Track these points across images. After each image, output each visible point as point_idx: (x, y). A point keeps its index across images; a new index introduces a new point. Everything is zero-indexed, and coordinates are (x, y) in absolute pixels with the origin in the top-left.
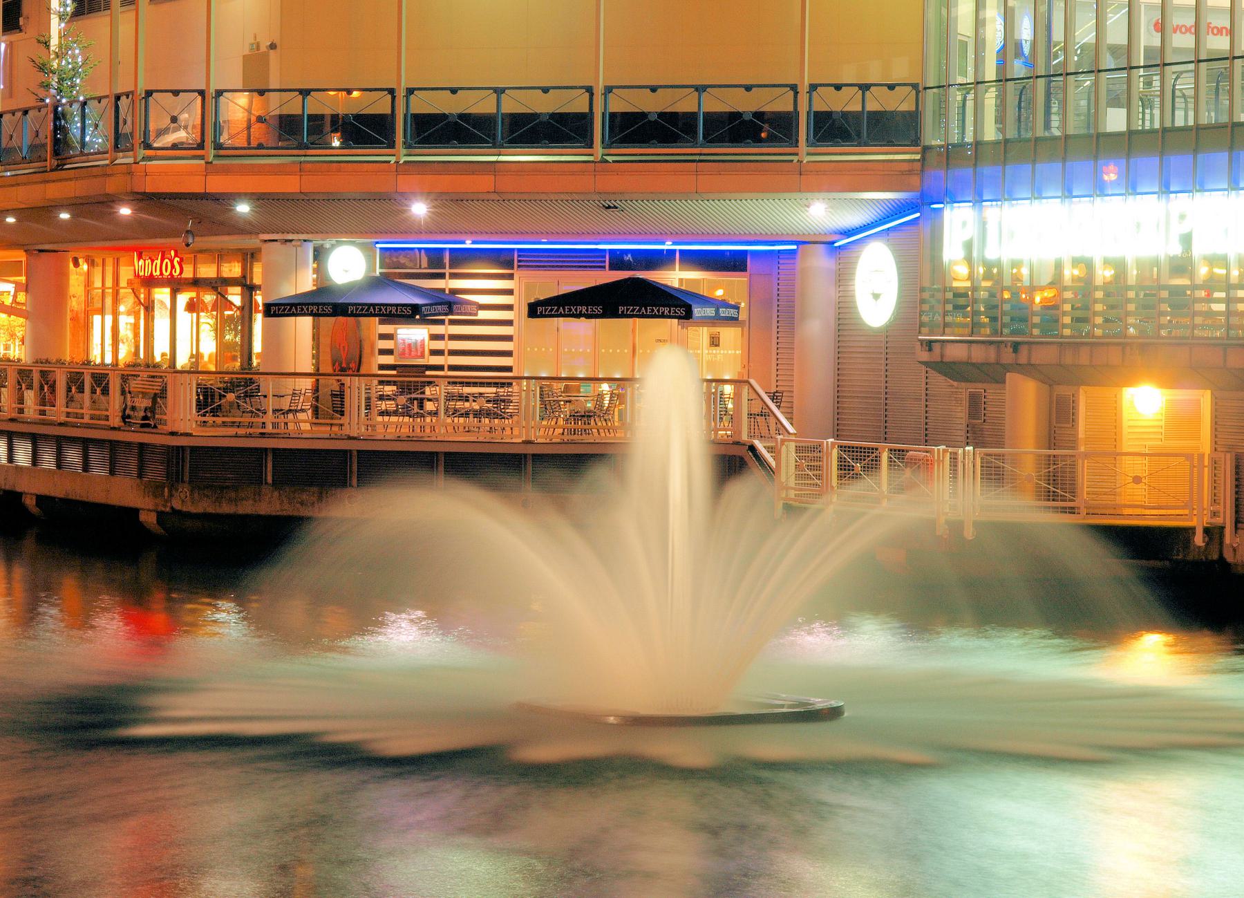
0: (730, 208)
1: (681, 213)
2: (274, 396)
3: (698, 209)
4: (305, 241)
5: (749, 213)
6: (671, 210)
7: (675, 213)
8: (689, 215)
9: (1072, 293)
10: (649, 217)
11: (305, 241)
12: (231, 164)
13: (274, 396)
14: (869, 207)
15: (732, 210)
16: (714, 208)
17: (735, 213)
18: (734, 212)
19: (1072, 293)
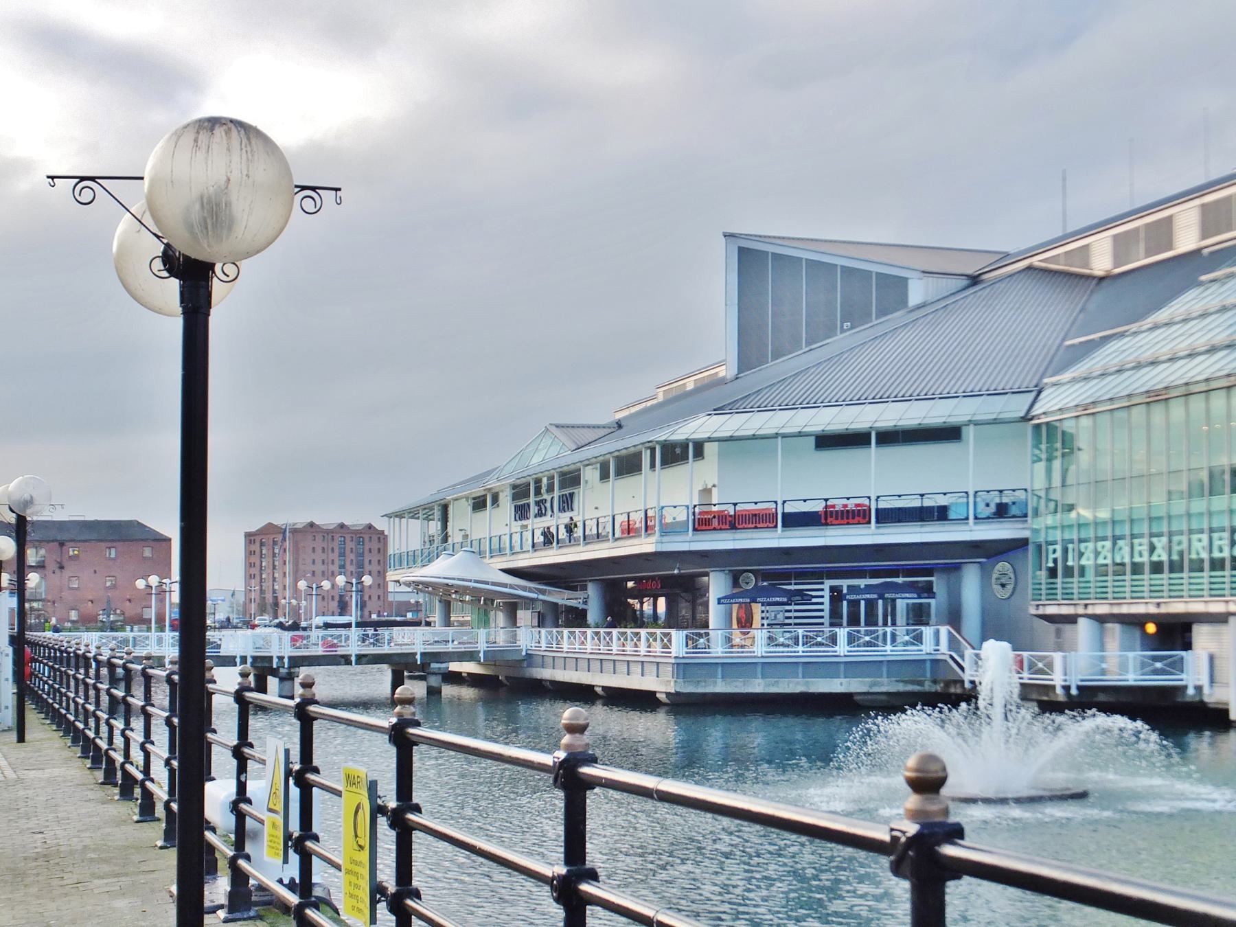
0: (878, 373)
1: (881, 377)
2: (142, 178)
3: (985, 339)
4: (456, 500)
5: (953, 359)
6: (956, 335)
7: (824, 383)
8: (936, 344)
9: (914, 815)
10: (848, 372)
11: (456, 500)
12: (848, 617)
13: (142, 178)
14: (925, 330)
15: (928, 346)
16: (991, 348)
17: (877, 382)
18: (875, 384)
19: (914, 815)
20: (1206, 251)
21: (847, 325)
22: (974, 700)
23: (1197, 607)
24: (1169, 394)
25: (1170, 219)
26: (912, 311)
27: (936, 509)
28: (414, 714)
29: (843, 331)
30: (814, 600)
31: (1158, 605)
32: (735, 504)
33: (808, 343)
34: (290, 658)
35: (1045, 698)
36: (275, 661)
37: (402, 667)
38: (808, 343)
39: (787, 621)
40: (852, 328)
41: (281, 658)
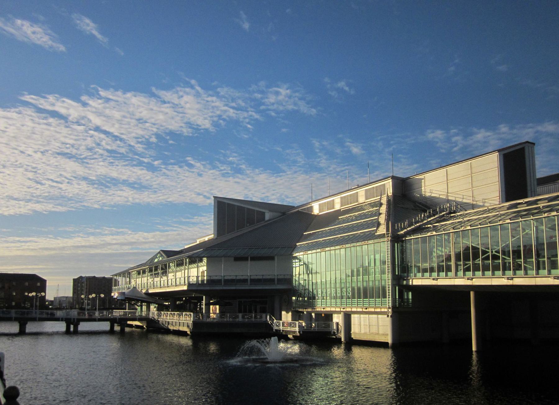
20: (342, 210)
21: (248, 225)
22: (54, 237)
23: (333, 309)
24: (505, 221)
25: (333, 200)
26: (266, 222)
27: (84, 280)
28: (221, 167)
29: (247, 226)
30: (233, 305)
31: (324, 308)
32: (236, 276)
33: (237, 230)
34: (77, 319)
35: (294, 335)
36: (72, 320)
37: (113, 321)
38: (237, 230)
39: (226, 311)
40: (250, 225)
41: (74, 319)
